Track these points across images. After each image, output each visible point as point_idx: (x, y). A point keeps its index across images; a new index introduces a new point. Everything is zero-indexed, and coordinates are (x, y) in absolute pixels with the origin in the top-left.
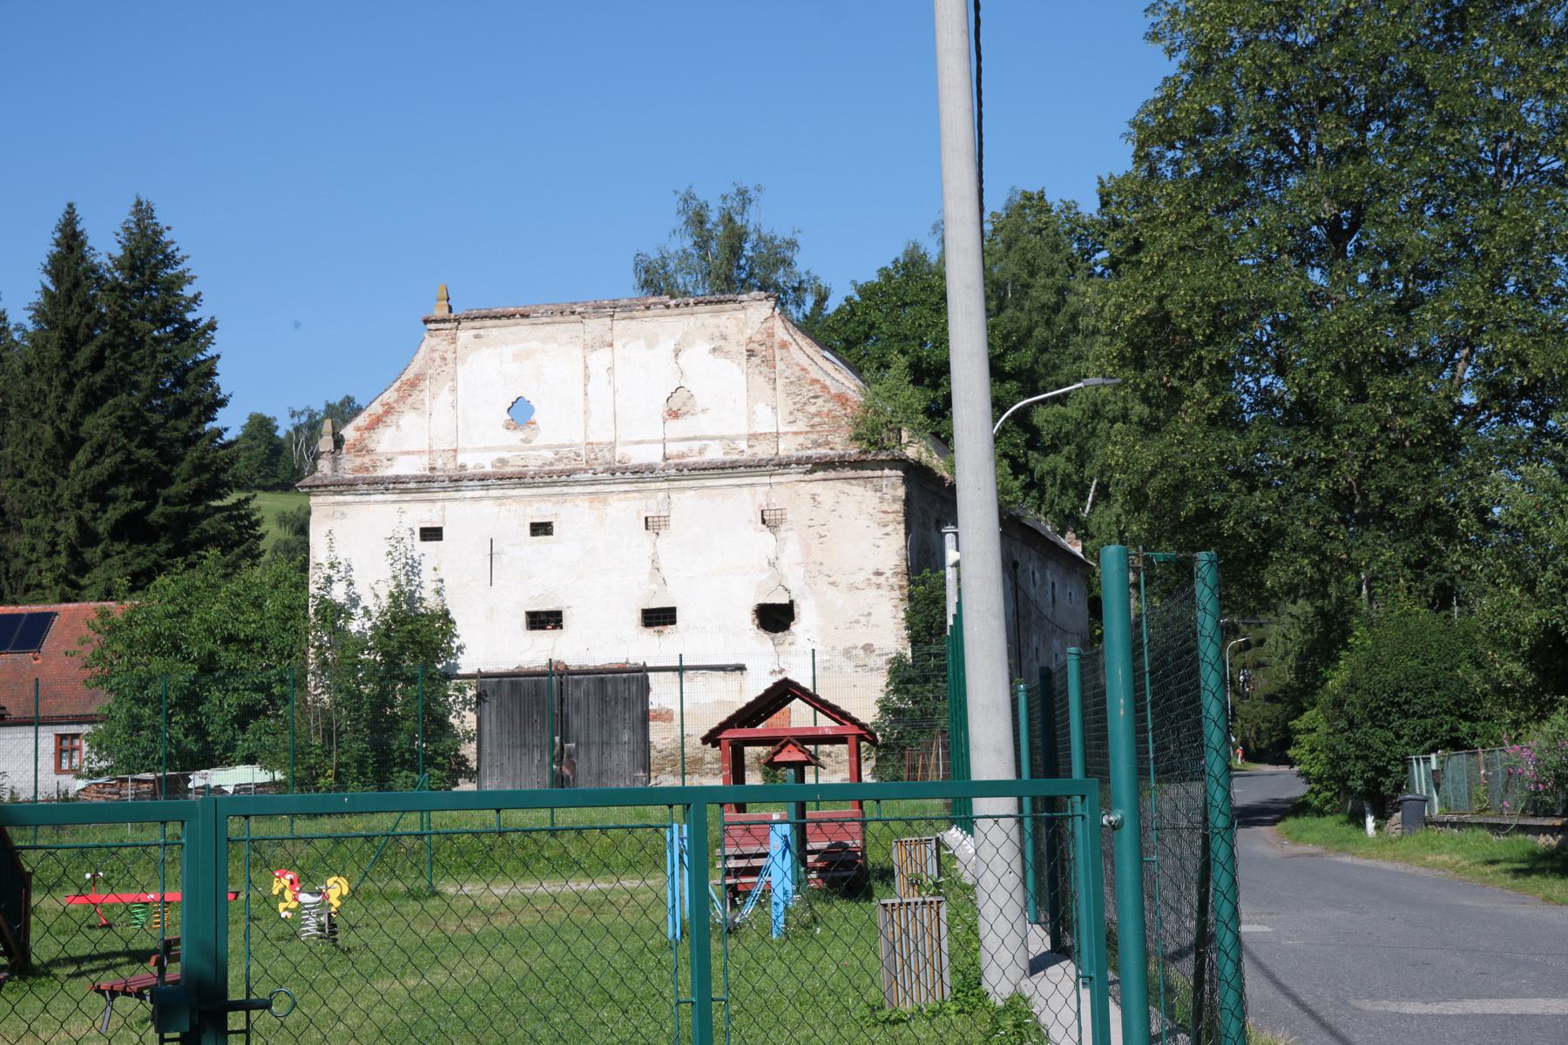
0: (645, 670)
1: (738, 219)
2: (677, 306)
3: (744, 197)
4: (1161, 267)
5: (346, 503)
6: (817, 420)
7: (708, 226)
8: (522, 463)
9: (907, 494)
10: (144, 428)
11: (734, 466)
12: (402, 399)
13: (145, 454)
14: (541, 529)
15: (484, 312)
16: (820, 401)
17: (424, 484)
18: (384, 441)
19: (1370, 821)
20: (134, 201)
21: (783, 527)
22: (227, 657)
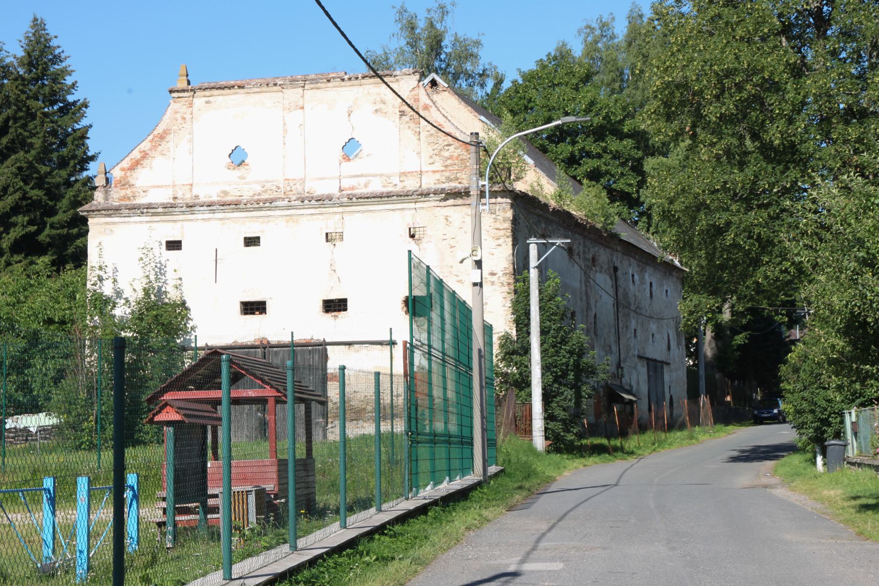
0: (324, 344)
1: (438, 26)
2: (350, 79)
3: (444, 11)
4: (683, 45)
5: (114, 223)
6: (449, 162)
7: (418, 31)
8: (239, 194)
9: (514, 217)
10: (35, 175)
11: (389, 195)
12: (154, 147)
13: (36, 194)
14: (252, 242)
15: (212, 85)
16: (452, 148)
17: (169, 209)
18: (142, 178)
19: (819, 459)
20: (32, 18)
21: (424, 241)
22: (45, 334)
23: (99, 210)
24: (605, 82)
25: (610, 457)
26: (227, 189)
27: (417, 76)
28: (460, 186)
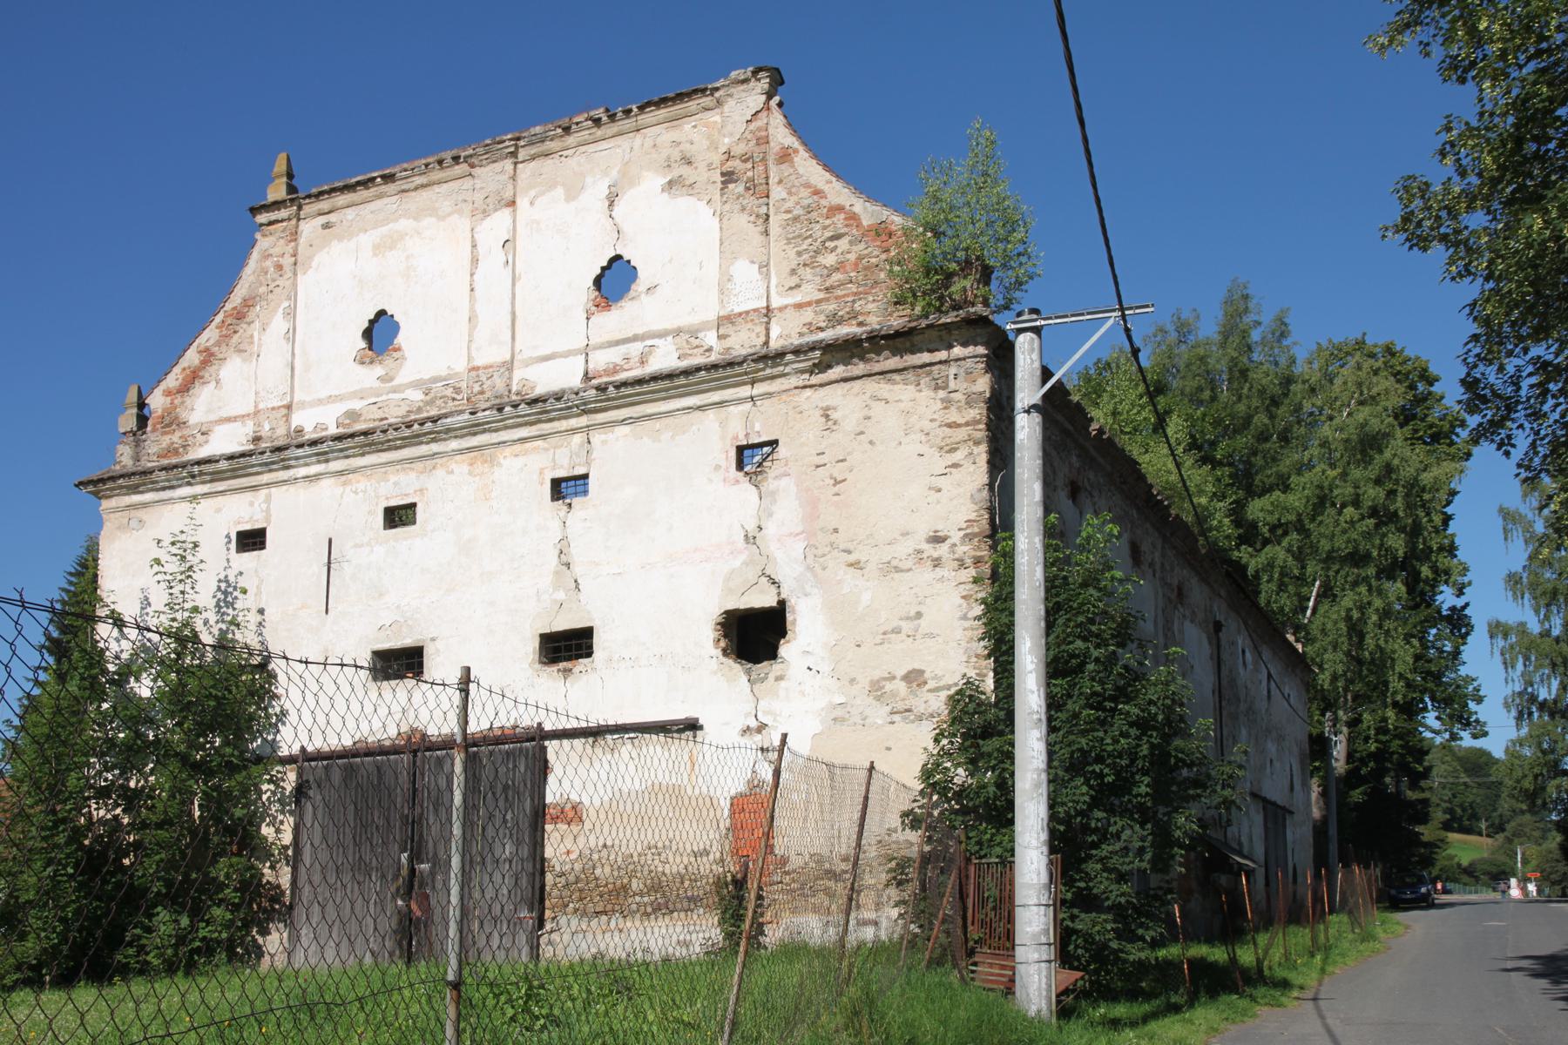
0: (539, 736)
5: (145, 505)
6: (837, 277)
12: (225, 339)
14: (398, 516)
16: (843, 244)
18: (201, 406)
23: (113, 478)
24: (1188, 390)
25: (1243, 1003)
26: (357, 405)
27: (764, 83)
28: (857, 330)
